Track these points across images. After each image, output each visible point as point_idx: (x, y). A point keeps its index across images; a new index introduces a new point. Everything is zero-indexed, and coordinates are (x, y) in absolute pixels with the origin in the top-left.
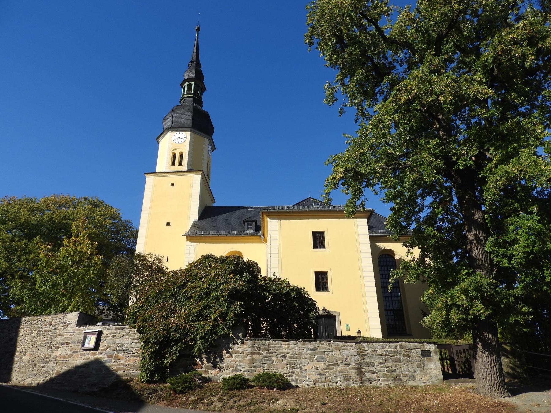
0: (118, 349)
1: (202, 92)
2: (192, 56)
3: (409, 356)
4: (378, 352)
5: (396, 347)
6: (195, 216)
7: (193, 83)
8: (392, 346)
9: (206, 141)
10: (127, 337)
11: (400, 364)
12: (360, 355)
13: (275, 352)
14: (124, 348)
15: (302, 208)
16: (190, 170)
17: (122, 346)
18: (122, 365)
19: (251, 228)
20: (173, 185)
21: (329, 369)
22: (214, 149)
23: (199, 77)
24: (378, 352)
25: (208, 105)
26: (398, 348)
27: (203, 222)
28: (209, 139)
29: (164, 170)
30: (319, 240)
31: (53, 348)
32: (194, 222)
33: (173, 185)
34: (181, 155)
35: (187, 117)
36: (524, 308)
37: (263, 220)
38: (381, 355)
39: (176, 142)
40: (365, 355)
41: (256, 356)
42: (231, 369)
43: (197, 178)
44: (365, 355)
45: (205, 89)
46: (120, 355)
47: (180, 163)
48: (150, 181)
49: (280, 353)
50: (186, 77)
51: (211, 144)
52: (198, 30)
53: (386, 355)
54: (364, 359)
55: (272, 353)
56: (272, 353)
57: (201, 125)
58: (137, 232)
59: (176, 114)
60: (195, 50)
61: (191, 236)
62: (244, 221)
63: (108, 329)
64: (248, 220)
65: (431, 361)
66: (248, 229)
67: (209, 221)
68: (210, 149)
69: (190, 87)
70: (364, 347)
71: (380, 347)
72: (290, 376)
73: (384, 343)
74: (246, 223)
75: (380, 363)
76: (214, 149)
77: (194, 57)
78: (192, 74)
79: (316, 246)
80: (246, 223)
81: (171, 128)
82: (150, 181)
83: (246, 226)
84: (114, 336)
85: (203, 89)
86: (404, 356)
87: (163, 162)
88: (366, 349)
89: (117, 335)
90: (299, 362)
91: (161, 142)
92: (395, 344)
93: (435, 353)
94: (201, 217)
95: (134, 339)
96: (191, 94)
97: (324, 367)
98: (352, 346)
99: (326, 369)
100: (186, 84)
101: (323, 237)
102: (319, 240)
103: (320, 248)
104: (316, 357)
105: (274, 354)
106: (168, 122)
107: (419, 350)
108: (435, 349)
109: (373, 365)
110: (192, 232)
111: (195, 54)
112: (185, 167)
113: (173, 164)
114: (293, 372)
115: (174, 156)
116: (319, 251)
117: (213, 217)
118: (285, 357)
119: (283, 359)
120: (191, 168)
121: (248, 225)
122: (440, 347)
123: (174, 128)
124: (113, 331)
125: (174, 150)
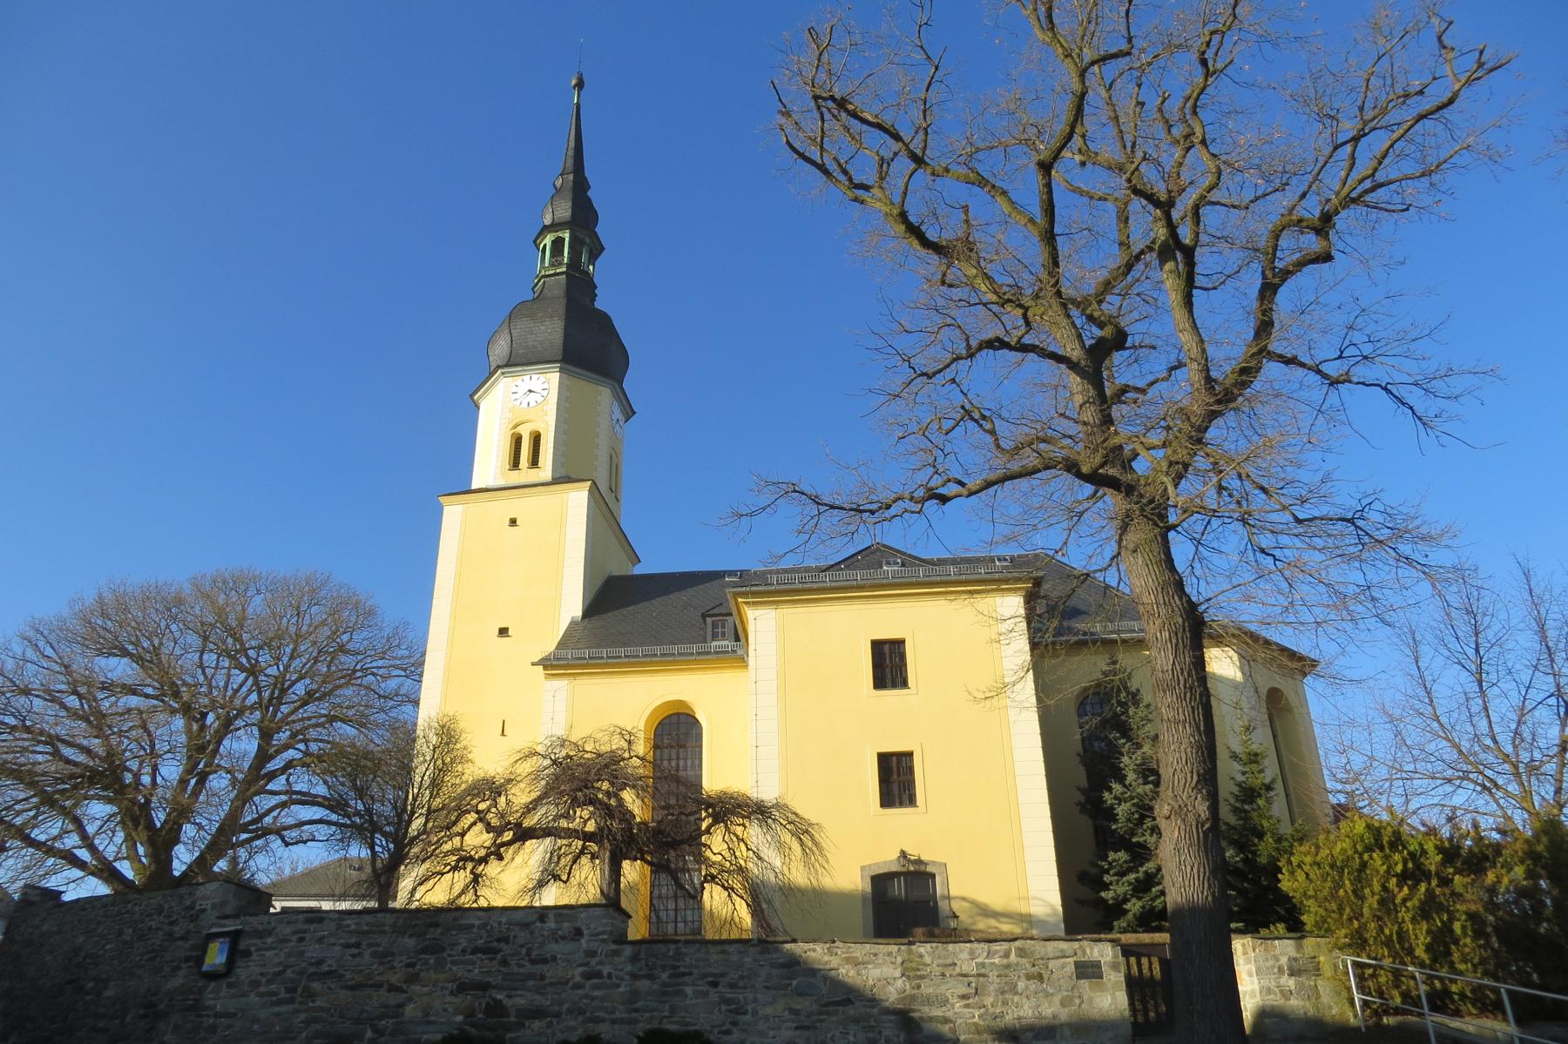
0: (312, 970)
1: (593, 257)
2: (561, 156)
3: (1040, 977)
4: (958, 970)
5: (1007, 955)
6: (572, 605)
7: (567, 235)
8: (996, 952)
9: (604, 394)
10: (332, 940)
11: (1016, 998)
12: (908, 978)
13: (690, 974)
14: (325, 968)
15: (844, 575)
16: (562, 478)
17: (319, 963)
18: (321, 1009)
19: (723, 634)
20: (513, 522)
21: (828, 1013)
22: (629, 412)
23: (583, 218)
24: (958, 970)
25: (613, 297)
26: (1013, 955)
27: (597, 621)
28: (613, 390)
29: (491, 483)
30: (889, 665)
31: (166, 969)
32: (573, 623)
33: (513, 522)
34: (536, 439)
35: (551, 330)
36: (164, 770)
37: (1016, 590)
38: (965, 976)
39: (522, 401)
40: (922, 977)
41: (644, 985)
42: (580, 1019)
43: (577, 498)
44: (922, 977)
45: (603, 249)
46: (316, 985)
47: (534, 462)
48: (454, 513)
49: (704, 976)
50: (548, 221)
51: (618, 399)
52: (580, 85)
53: (979, 975)
54: (919, 987)
55: (684, 974)
56: (684, 974)
57: (590, 348)
58: (421, 663)
59: (521, 326)
60: (572, 144)
61: (553, 664)
62: (704, 616)
63: (289, 923)
64: (716, 611)
65: (1102, 989)
66: (715, 637)
67: (612, 617)
68: (618, 415)
69: (558, 243)
70: (921, 956)
71: (965, 955)
72: (728, 1032)
73: (975, 945)
74: (709, 620)
75: (964, 997)
76: (629, 412)
77: (570, 163)
78: (564, 211)
79: (880, 682)
80: (709, 620)
81: (507, 365)
82: (454, 513)
83: (709, 629)
84: (301, 940)
85: (597, 251)
86: (1029, 977)
87: (488, 465)
88: (928, 960)
89: (308, 936)
90: (750, 996)
91: (483, 405)
92: (1005, 946)
93: (1115, 966)
94: (591, 610)
95: (349, 946)
96: (561, 264)
97: (815, 1007)
98: (890, 954)
99: (821, 1013)
100: (548, 240)
101: (903, 656)
102: (889, 665)
103: (894, 686)
104: (794, 983)
105: (686, 979)
106: (501, 348)
107: (1071, 960)
108: (1115, 956)
109: (945, 1002)
110: (563, 653)
111: (571, 153)
112: (545, 471)
113: (515, 464)
114: (735, 1024)
115: (517, 441)
116: (891, 696)
117: (635, 609)
118: (715, 985)
119: (712, 990)
120: (563, 472)
121: (714, 625)
122: (1127, 951)
123: (518, 360)
124: (300, 926)
125: (516, 426)
